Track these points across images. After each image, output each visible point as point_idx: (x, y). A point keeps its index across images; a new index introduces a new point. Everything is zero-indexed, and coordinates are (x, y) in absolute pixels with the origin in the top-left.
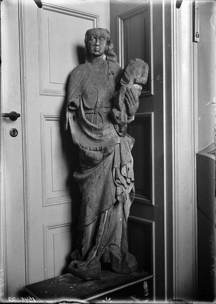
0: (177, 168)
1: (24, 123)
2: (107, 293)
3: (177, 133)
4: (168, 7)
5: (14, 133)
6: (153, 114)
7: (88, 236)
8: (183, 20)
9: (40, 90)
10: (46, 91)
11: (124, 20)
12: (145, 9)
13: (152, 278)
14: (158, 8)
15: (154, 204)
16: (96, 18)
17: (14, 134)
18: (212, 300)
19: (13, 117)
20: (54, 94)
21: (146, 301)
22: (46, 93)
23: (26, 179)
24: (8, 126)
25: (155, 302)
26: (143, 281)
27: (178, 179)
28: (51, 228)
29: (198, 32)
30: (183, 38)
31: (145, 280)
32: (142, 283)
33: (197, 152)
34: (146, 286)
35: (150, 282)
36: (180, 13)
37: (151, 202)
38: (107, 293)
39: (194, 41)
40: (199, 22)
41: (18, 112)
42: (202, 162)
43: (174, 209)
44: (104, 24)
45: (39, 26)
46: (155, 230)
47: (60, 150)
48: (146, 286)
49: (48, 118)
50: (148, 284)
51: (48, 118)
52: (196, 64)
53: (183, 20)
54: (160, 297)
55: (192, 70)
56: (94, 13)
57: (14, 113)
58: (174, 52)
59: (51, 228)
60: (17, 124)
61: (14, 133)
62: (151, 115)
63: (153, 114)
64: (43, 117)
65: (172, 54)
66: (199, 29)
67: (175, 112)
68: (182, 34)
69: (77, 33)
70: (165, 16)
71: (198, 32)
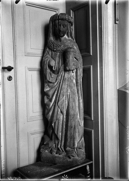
0: (106, 98)
1: (16, 73)
2: (65, 172)
3: (106, 85)
4: (100, 5)
5: (10, 78)
6: (92, 66)
7: (49, 115)
8: (109, 12)
9: (25, 52)
10: (28, 53)
11: (74, 11)
12: (86, 5)
13: (92, 163)
14: (94, 5)
15: (93, 119)
16: (57, 10)
17: (10, 79)
18: (127, 2)
19: (9, 69)
20: (34, 55)
21: (89, 180)
22: (28, 55)
23: (17, 106)
24: (7, 74)
25: (94, 180)
26: (86, 165)
27: (107, 104)
28: (32, 134)
29: (118, 18)
30: (109, 21)
31: (88, 165)
32: (86, 166)
33: (118, 88)
34: (88, 168)
35: (91, 166)
36: (107, 6)
37: (91, 118)
38: (65, 172)
39: (115, 23)
40: (118, 12)
41: (12, 66)
42: (122, 95)
43: (105, 166)
44: (62, 10)
45: (24, 15)
46: (100, 115)
47: (41, 106)
48: (88, 168)
49: (31, 70)
50: (89, 167)
51: (31, 70)
52: (117, 60)
53: (109, 12)
54: (97, 176)
55: (114, 39)
56: (57, 7)
57: (10, 67)
58: (104, 45)
59: (32, 134)
60: (11, 74)
61: (10, 78)
62: (90, 67)
63: (92, 66)
64: (27, 69)
65: (103, 31)
66: (118, 16)
67: (106, 109)
68: (109, 19)
69: (47, 16)
70: (98, 9)
71: (118, 18)
